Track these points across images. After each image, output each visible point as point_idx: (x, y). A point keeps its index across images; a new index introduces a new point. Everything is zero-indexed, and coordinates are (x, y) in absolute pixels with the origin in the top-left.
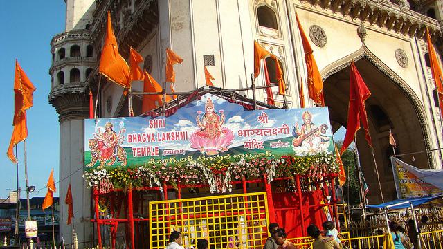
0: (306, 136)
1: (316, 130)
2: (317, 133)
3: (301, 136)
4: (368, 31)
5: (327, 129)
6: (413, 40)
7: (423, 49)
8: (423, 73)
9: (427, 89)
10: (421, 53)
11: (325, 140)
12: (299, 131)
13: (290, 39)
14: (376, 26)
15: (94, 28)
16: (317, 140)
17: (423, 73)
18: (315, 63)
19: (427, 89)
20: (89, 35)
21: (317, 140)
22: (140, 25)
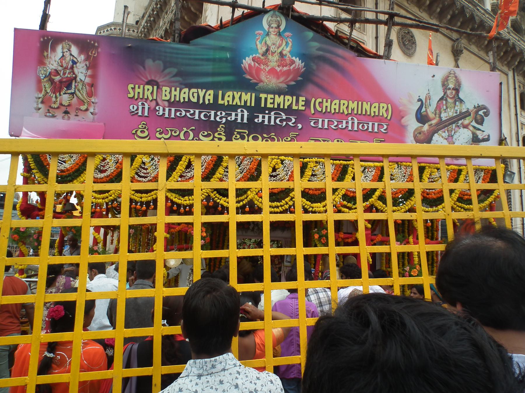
0: (442, 125)
1: (465, 115)
2: (466, 121)
3: (434, 122)
4: (465, 51)
5: (487, 114)
6: (511, 74)
7: (520, 87)
8: (516, 115)
9: (517, 133)
10: (517, 90)
11: (480, 137)
12: (431, 111)
13: (374, 36)
14: (473, 48)
15: (143, 23)
16: (463, 135)
17: (516, 115)
18: (39, 363)
19: (517, 133)
20: (137, 32)
21: (463, 135)
22: (190, 5)
